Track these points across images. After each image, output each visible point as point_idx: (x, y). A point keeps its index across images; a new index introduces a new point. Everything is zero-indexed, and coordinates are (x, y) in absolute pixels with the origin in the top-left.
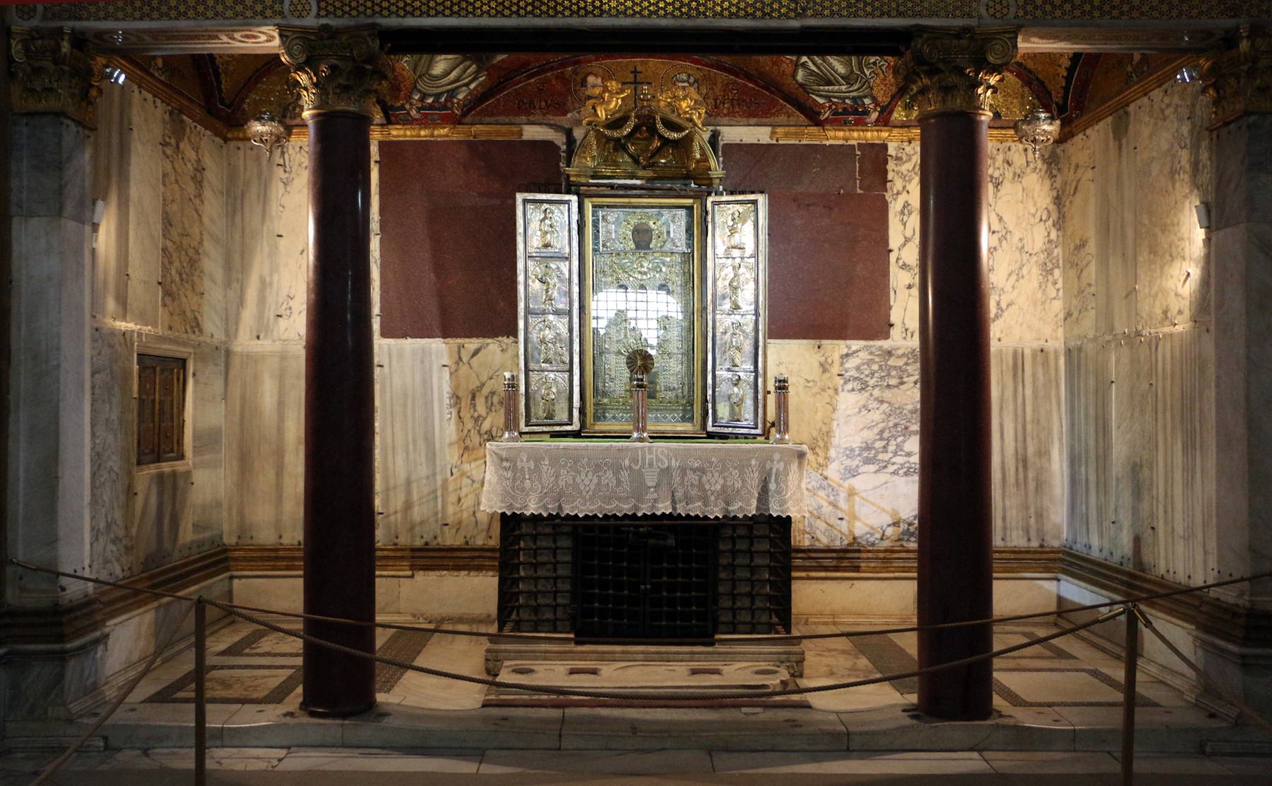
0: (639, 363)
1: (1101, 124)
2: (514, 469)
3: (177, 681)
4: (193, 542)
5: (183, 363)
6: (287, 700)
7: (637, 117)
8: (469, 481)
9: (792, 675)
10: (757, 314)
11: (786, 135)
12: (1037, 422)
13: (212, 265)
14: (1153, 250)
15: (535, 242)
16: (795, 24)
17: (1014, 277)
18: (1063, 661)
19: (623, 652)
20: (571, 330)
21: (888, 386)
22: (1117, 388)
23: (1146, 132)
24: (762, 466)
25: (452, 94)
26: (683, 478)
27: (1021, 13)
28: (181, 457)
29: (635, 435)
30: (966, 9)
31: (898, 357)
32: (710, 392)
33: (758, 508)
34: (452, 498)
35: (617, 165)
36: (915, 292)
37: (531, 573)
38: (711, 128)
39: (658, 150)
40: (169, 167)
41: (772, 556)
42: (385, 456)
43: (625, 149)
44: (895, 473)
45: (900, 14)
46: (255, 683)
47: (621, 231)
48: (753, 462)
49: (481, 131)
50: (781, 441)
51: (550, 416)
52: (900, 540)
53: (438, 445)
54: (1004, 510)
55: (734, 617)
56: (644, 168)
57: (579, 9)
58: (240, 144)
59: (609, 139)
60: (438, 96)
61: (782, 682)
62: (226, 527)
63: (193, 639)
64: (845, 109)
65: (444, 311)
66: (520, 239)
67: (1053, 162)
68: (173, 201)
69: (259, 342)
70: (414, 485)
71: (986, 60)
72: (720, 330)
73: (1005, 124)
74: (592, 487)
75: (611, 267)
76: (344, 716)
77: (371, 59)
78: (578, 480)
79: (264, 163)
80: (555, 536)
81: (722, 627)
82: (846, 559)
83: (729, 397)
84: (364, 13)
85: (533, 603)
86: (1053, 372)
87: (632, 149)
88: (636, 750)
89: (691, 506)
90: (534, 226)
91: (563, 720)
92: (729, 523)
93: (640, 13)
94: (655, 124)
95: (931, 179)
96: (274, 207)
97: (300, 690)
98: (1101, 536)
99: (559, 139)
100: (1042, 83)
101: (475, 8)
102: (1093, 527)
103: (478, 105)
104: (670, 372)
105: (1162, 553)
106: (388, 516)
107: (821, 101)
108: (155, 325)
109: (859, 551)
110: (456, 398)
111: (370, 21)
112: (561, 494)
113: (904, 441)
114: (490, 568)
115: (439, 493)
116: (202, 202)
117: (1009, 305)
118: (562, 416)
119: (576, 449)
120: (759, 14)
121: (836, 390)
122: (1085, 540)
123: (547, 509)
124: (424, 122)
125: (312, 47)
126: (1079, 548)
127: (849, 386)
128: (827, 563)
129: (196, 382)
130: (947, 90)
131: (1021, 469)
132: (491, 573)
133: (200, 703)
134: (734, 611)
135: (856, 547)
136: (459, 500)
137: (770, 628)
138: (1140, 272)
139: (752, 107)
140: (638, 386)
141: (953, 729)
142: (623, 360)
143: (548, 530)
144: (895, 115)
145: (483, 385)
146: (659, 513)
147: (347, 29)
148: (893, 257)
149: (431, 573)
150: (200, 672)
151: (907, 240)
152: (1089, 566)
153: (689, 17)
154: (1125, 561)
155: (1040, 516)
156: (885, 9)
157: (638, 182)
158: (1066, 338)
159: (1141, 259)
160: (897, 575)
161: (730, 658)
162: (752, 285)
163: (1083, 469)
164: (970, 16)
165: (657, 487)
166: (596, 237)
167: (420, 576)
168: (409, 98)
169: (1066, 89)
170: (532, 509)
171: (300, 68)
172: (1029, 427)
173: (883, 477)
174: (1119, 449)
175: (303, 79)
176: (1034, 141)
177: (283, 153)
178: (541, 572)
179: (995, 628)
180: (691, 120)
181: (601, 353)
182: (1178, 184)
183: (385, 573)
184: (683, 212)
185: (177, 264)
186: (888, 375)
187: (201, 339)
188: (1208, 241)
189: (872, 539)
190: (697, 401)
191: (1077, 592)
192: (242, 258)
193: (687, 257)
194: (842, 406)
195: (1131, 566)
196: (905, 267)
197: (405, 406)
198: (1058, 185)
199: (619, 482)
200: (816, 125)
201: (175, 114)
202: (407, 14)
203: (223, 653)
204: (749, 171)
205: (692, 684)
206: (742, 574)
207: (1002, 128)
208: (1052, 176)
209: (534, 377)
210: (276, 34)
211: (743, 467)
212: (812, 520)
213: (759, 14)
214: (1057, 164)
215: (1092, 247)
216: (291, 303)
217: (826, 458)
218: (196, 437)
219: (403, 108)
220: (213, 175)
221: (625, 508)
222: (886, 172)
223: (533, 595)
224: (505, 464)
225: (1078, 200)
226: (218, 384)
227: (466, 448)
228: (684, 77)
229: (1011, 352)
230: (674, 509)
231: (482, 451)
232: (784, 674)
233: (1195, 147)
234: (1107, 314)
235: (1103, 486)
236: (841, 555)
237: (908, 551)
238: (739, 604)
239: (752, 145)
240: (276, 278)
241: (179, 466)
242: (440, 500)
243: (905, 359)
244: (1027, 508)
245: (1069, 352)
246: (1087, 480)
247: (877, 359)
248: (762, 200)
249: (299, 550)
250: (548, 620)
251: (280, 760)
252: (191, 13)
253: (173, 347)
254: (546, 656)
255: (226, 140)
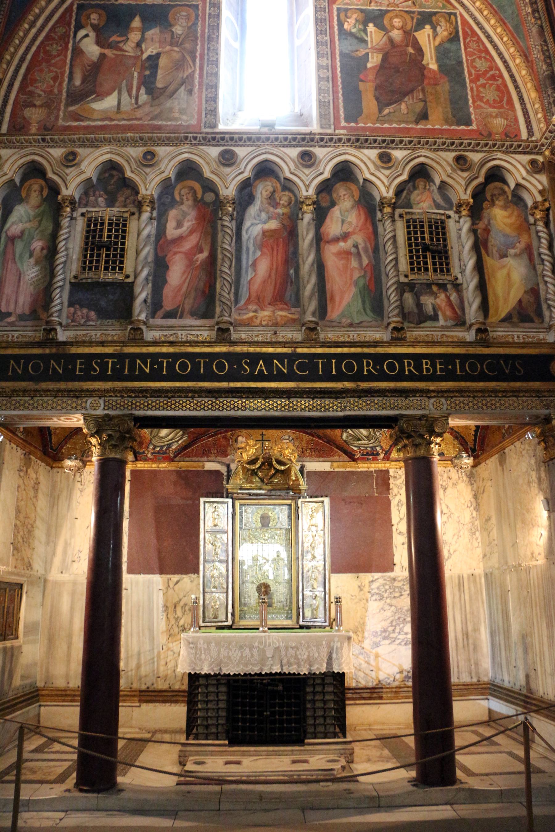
0: (263, 590)
1: (493, 458)
2: (196, 648)
3: (6, 769)
4: (20, 685)
5: (21, 586)
6: (67, 781)
7: (263, 458)
8: (172, 653)
9: (348, 762)
10: (325, 561)
11: (338, 466)
12: (472, 613)
13: (40, 533)
14: (523, 522)
15: (210, 523)
16: (341, 414)
17: (456, 537)
18: (493, 747)
19: (255, 751)
20: (227, 571)
21: (394, 597)
22: (512, 594)
23: (514, 462)
24: (329, 643)
25: (169, 446)
26: (286, 653)
27: (449, 408)
28: (17, 638)
29: (261, 629)
30: (423, 406)
31: (399, 581)
32: (301, 603)
33: (327, 668)
34: (163, 662)
35: (252, 482)
36: (406, 546)
37: (204, 706)
38: (300, 463)
39: (274, 475)
40: (22, 481)
41: (335, 694)
42: (127, 638)
43: (256, 474)
44: (400, 644)
45: (392, 409)
46: (50, 771)
47: (254, 517)
48: (324, 643)
49: (184, 465)
50: (338, 630)
51: (216, 617)
52: (403, 681)
53: (155, 633)
54: (458, 662)
55: (315, 729)
56: (266, 484)
57: (235, 407)
58: (59, 470)
59: (248, 470)
60: (162, 447)
61: (342, 767)
62: (38, 678)
63: (17, 743)
64: (367, 453)
65: (161, 559)
66: (202, 522)
67: (471, 476)
68: (22, 500)
69: (62, 575)
70: (142, 655)
71: (434, 430)
72: (305, 570)
73: (447, 459)
74: (238, 658)
75: (249, 537)
76: (99, 791)
77: (129, 431)
78: (230, 654)
79: (71, 480)
80: (217, 686)
81: (308, 735)
82: (374, 693)
83: (311, 606)
84: (127, 408)
85: (205, 723)
86: (479, 586)
87: (260, 474)
88: (263, 810)
89: (291, 668)
90: (209, 515)
91: (221, 792)
92: (312, 676)
93: (265, 409)
94: (272, 461)
95: (411, 483)
96: (74, 503)
97: (75, 775)
98: (509, 675)
99: (224, 470)
100: (463, 438)
101: (182, 406)
102: (505, 669)
103: (183, 451)
104: (280, 593)
105: (540, 682)
106: (127, 672)
107: (355, 449)
108: (8, 565)
109: (382, 688)
110: (166, 607)
111: (130, 412)
112: (221, 662)
113: (403, 627)
114: (183, 701)
115: (155, 659)
116: (37, 500)
117: (454, 552)
118: (222, 617)
119: (229, 637)
120: (323, 409)
121: (367, 600)
122: (501, 677)
123: (213, 671)
124: (154, 460)
125: (100, 425)
126: (498, 681)
127: (374, 598)
128: (365, 695)
129: (27, 597)
130: (416, 446)
131: (465, 640)
132: (183, 704)
133: (18, 783)
134: (315, 725)
135: (380, 686)
136: (166, 663)
137: (335, 735)
138: (518, 533)
139: (321, 453)
140: (263, 602)
141: (436, 792)
142: (255, 587)
143: (214, 682)
144: (392, 455)
145: (180, 600)
146: (274, 672)
147: (119, 416)
148: (394, 528)
149: (150, 704)
150: (20, 761)
151: (401, 519)
152: (505, 692)
153: (289, 411)
154: (522, 688)
155: (477, 664)
156: (384, 406)
157: (263, 492)
158: (484, 568)
159: (518, 526)
160: (403, 700)
161: (313, 753)
162: (322, 546)
163: (497, 638)
164: (425, 409)
165: (273, 657)
166: (241, 521)
167: (144, 706)
168: (147, 447)
169: (475, 441)
170: (205, 670)
171: (92, 435)
172: (468, 616)
173: (393, 646)
174: (515, 627)
175: (94, 441)
176: (461, 468)
177: (81, 475)
178: (210, 706)
179: (455, 730)
180: (290, 460)
181: (243, 583)
182: (532, 489)
183: (125, 704)
184: (286, 507)
185: (21, 533)
186: (394, 591)
187: (31, 573)
188: (549, 517)
189: (388, 681)
190: (294, 607)
191: (501, 707)
192: (56, 529)
193: (289, 531)
194: (370, 609)
195: (525, 691)
196: (400, 533)
197: (138, 611)
198: (475, 488)
199: (252, 656)
200: (354, 461)
201: (27, 454)
202: (148, 409)
203: (32, 751)
204: (321, 485)
205: (293, 769)
206: (319, 705)
207: (445, 460)
208: (472, 484)
209: (208, 596)
210: (82, 418)
211: (318, 646)
212: (356, 672)
213: (323, 409)
214: (474, 478)
215: (494, 520)
216: (80, 555)
217: (363, 637)
218: (25, 627)
219: (144, 453)
220: (43, 487)
221: (255, 670)
222: (389, 484)
223: (206, 718)
224: (191, 645)
225: (485, 494)
226: (39, 598)
227: (171, 635)
228: (287, 437)
229: (457, 576)
230: (282, 669)
231: (179, 636)
232: (343, 762)
233: (538, 470)
234: (504, 556)
235: (508, 647)
236: (373, 691)
237: (408, 687)
238: (317, 722)
239: (321, 472)
240: (73, 540)
241: (15, 643)
242: (156, 664)
243: (402, 582)
244: (469, 660)
245: (486, 575)
246: (500, 644)
247: (388, 583)
248: (326, 500)
249: (78, 691)
250: (213, 733)
251: (61, 820)
252: (40, 407)
253: (17, 578)
254: (212, 754)
255: (52, 468)
